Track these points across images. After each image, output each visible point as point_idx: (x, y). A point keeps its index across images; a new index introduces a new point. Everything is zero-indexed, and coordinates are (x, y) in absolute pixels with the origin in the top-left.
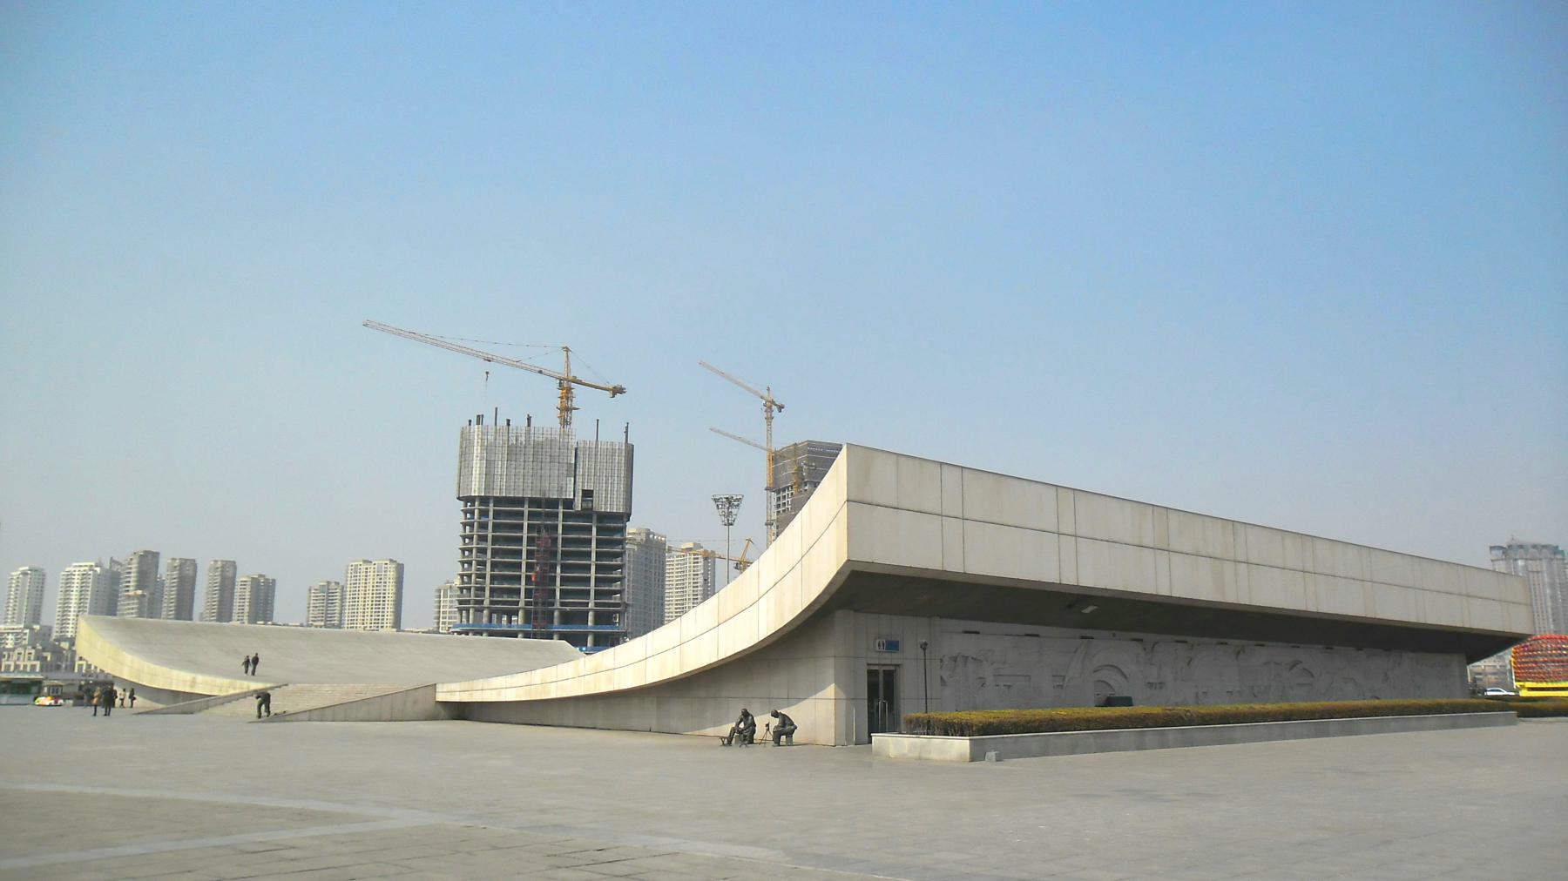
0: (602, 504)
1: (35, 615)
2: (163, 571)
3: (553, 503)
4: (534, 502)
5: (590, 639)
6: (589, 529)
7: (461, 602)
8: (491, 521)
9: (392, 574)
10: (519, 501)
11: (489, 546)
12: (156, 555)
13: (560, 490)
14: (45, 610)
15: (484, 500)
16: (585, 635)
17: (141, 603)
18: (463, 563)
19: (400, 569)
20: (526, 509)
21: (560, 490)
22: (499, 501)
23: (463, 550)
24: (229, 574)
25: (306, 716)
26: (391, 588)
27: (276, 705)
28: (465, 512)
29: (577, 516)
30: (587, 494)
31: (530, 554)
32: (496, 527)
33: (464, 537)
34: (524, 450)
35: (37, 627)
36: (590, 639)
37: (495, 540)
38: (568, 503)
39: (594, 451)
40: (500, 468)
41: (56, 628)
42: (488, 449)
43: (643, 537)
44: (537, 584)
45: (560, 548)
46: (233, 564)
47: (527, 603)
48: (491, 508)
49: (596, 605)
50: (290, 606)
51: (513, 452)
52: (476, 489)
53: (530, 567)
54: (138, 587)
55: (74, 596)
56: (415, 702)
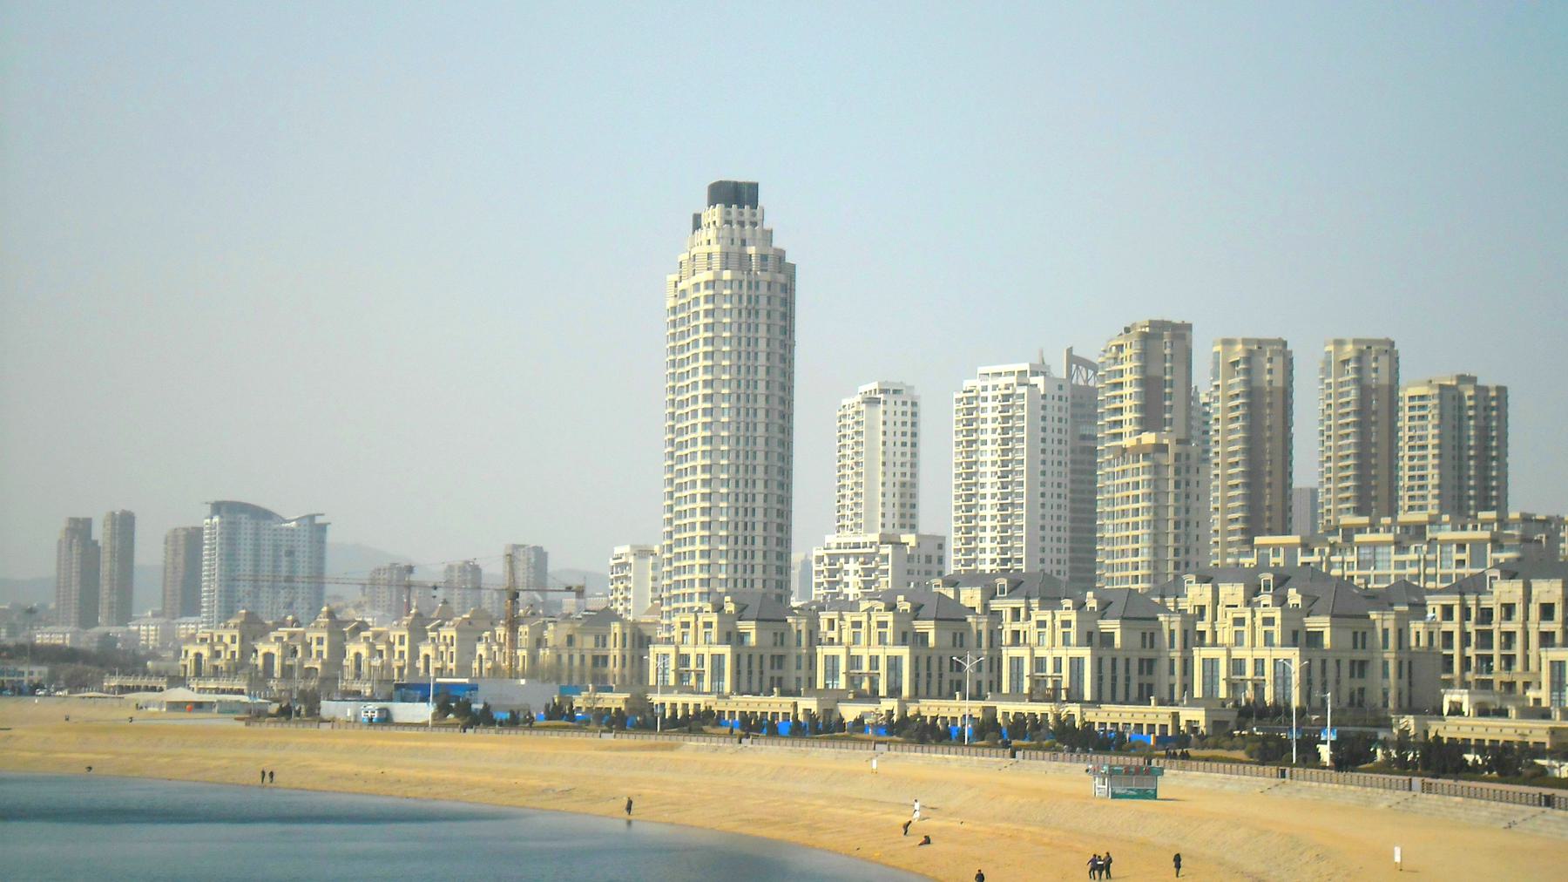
1: (908, 514)
2: (1203, 380)
12: (1181, 332)
17: (1157, 469)
24: (1379, 378)
35: (909, 539)
41: (954, 543)
46: (1389, 349)
50: (909, 566)
54: (1145, 424)
55: (989, 454)
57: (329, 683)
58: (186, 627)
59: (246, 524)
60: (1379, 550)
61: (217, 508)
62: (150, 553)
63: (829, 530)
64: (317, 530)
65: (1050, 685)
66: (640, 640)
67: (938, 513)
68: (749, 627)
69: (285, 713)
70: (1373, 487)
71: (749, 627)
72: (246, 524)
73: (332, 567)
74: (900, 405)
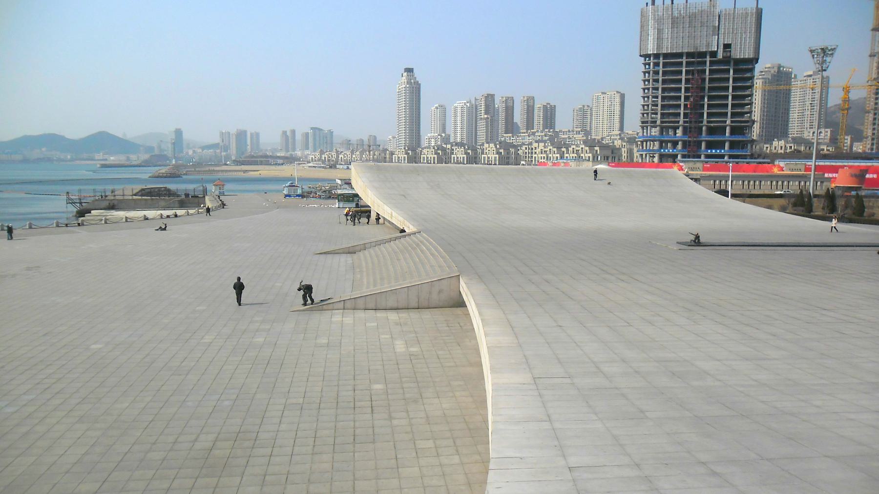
0: (738, 53)
1: (444, 131)
3: (703, 55)
4: (689, 55)
5: (727, 145)
6: (728, 71)
7: (643, 122)
8: (661, 69)
9: (618, 99)
10: (680, 55)
11: (660, 85)
12: (493, 96)
13: (708, 45)
14: (447, 128)
15: (657, 56)
16: (724, 142)
17: (487, 122)
18: (644, 97)
19: (622, 96)
20: (684, 60)
21: (708, 45)
22: (666, 56)
23: (644, 89)
25: (341, 305)
26: (617, 108)
27: (317, 295)
28: (645, 64)
29: (720, 62)
30: (727, 46)
31: (687, 90)
32: (664, 73)
33: (644, 81)
34: (693, 20)
36: (727, 145)
37: (664, 82)
38: (714, 54)
39: (733, 16)
40: (667, 33)
41: (452, 135)
42: (659, 21)
43: (776, 69)
44: (691, 109)
45: (707, 85)
46: (533, 98)
47: (685, 122)
48: (661, 61)
49: (732, 122)
51: (675, 21)
52: (651, 49)
53: (687, 98)
54: (486, 114)
55: (459, 118)
56: (440, 292)
57: (337, 162)
58: (307, 152)
59: (317, 132)
60: (228, 187)
61: (312, 128)
62: (298, 137)
63: (429, 135)
64: (331, 133)
65: (624, 155)
66: (392, 154)
67: (450, 130)
68: (410, 152)
69: (331, 167)
70: (530, 124)
71: (410, 152)
72: (317, 132)
73: (335, 140)
74: (443, 109)
